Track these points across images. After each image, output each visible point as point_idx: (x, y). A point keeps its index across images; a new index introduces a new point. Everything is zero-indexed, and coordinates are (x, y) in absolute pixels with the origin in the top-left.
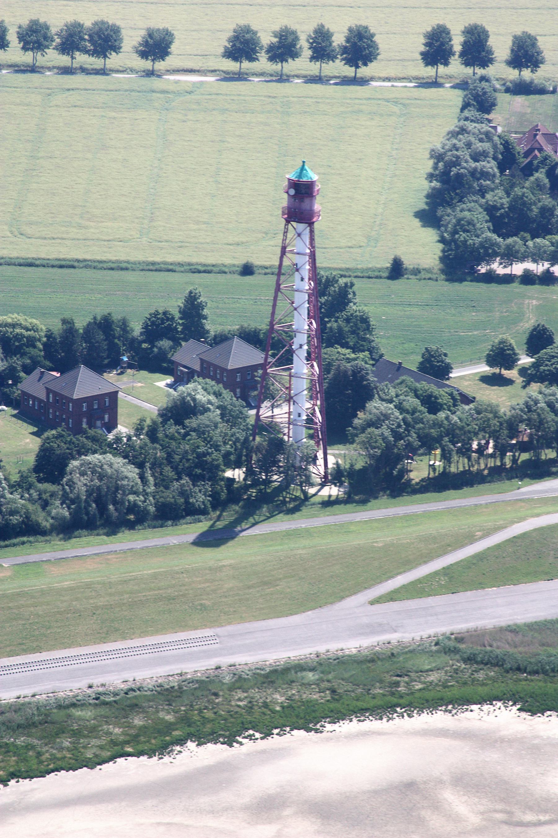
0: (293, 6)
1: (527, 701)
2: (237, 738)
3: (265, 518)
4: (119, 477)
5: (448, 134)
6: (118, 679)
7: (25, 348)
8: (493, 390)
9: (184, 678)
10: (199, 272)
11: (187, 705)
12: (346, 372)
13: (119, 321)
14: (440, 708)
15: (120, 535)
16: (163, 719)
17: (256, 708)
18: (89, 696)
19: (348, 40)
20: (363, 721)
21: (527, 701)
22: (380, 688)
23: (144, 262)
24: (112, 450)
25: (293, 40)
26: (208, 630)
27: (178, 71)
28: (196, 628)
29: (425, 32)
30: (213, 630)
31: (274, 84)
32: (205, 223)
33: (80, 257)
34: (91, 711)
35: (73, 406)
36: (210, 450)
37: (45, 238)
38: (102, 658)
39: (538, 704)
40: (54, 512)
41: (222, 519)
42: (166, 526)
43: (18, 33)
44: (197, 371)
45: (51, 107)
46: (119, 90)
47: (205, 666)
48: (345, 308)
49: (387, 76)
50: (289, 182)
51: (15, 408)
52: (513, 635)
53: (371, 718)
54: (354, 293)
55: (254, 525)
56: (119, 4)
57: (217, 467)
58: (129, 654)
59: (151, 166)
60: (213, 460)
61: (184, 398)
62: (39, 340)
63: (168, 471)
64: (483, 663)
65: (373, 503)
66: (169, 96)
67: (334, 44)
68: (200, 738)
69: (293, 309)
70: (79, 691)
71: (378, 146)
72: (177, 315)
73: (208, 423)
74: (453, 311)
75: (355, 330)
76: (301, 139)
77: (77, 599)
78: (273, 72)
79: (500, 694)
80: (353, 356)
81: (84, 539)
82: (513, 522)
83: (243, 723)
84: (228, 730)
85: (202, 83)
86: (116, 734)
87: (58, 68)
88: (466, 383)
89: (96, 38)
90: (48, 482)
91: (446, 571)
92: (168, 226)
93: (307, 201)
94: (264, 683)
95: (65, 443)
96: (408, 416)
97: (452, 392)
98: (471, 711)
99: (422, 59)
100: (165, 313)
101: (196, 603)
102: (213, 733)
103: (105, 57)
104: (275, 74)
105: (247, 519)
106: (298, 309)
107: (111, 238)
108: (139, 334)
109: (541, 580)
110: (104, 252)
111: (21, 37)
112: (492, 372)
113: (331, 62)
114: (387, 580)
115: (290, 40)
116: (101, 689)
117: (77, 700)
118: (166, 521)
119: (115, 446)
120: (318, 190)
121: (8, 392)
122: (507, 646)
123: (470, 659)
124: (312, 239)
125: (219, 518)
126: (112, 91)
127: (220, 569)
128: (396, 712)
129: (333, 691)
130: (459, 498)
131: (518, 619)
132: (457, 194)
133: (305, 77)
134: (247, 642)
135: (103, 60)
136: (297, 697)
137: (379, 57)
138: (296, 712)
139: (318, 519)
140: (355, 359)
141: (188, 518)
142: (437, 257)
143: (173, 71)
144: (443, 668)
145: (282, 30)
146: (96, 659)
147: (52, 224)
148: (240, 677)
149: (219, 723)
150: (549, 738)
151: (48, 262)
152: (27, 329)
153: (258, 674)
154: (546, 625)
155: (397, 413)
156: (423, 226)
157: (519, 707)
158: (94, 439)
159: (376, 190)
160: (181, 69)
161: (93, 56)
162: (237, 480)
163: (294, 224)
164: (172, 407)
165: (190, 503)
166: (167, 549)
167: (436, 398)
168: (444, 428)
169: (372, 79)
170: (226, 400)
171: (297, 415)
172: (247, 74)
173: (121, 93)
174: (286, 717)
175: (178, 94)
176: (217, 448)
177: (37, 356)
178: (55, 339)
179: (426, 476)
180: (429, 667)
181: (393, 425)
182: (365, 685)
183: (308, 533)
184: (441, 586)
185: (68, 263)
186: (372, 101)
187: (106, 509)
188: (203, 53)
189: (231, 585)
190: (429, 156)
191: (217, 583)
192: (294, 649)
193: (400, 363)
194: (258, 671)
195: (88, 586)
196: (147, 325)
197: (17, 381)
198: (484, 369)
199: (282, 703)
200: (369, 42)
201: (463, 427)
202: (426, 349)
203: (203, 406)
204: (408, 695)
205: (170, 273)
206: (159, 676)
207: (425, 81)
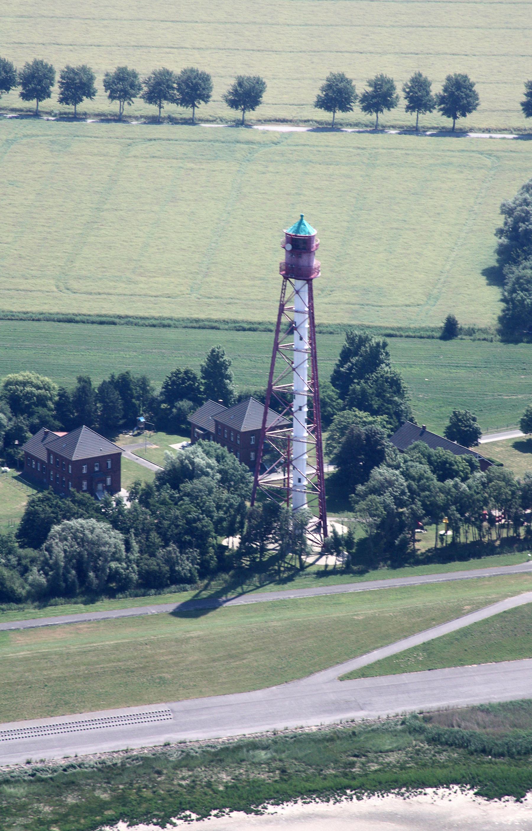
0: (405, 54)
1: (486, 785)
2: (172, 819)
3: (254, 588)
4: (98, 543)
5: (523, 188)
6: (59, 755)
7: (33, 407)
8: (524, 457)
9: (129, 754)
10: (244, 330)
11: (127, 783)
12: (359, 436)
13: (138, 381)
14: (393, 791)
15: (98, 604)
16: (99, 797)
17: (198, 787)
18: (26, 773)
19: (445, 90)
20: (309, 803)
21: (486, 785)
22: (333, 769)
23: (188, 319)
24: (99, 515)
25: (388, 89)
26: (163, 704)
27: (270, 121)
28: (150, 703)
29: (526, 81)
30: (169, 704)
31: (367, 135)
32: (261, 279)
33: (122, 313)
34: (24, 788)
35: (72, 468)
36: (201, 516)
37: (91, 294)
38: (46, 732)
39: (497, 788)
40: (30, 578)
41: (209, 588)
42: (149, 595)
43: (105, 81)
44: (212, 433)
45: (129, 157)
46: (203, 141)
47: (154, 742)
48: (375, 369)
49: (487, 127)
50: (287, 237)
51: (18, 470)
52: (484, 715)
53: (317, 800)
54: (387, 354)
55: (240, 595)
56: (224, 51)
57: (208, 534)
58: (76, 729)
59: (219, 219)
60: (203, 526)
61: (182, 462)
62: (51, 399)
63: (154, 536)
64: (447, 744)
65: (372, 573)
66: (254, 146)
67: (433, 94)
68: (133, 818)
69: (291, 369)
70: (16, 767)
71: (461, 200)
72: (199, 374)
73: (201, 487)
74: (501, 373)
75: (380, 393)
76: (382, 192)
77: (30, 670)
78: (368, 123)
79: (459, 777)
80: (371, 419)
81: (60, 607)
82: (506, 596)
83: (181, 803)
84: (164, 810)
85: (291, 133)
86: (45, 813)
87: (146, 117)
88: (498, 450)
89: (184, 86)
90: (30, 547)
91: (426, 647)
92: (221, 281)
93: (305, 257)
94: (212, 761)
95: (51, 507)
96: (413, 483)
97: (471, 459)
98: (425, 794)
99: (523, 109)
100: (186, 372)
101: (155, 676)
102: (148, 813)
103: (194, 106)
104: (371, 125)
105: (234, 589)
106: (296, 370)
107: (159, 293)
108: (159, 393)
109: (526, 657)
110: (149, 308)
111: (108, 85)
112: (527, 438)
113: (428, 112)
114: (361, 655)
115: (385, 89)
116: (39, 765)
117: (12, 777)
118: (148, 590)
119: (103, 510)
120: (317, 245)
121: (13, 453)
122: (476, 726)
123: (434, 740)
124: (311, 298)
125: (206, 588)
126: (195, 141)
127: (186, 641)
128: (345, 794)
129: (283, 771)
130: (461, 570)
131: (494, 698)
132: (524, 251)
133: (401, 127)
134: (203, 717)
135: (191, 110)
136: (244, 777)
137: (478, 108)
138: (239, 793)
139: (309, 590)
140: (370, 423)
141: (173, 586)
142: (495, 317)
143: (265, 121)
144: (404, 749)
145: (377, 79)
146: (40, 733)
147: (100, 279)
148: (188, 754)
149: (156, 803)
150: (501, 824)
151: (88, 318)
152: (38, 388)
153: (207, 752)
154: (522, 705)
155: (402, 480)
156: (489, 284)
157: (476, 790)
158: (81, 503)
159: (449, 246)
160: (273, 118)
161: (181, 105)
162: (230, 547)
163: (292, 280)
164: (170, 470)
165: (175, 571)
166: (143, 619)
167: (451, 464)
168: (451, 496)
169: (471, 130)
170: (228, 464)
171: (297, 480)
172: (341, 125)
173: (204, 143)
174: (228, 797)
175: (262, 144)
176: (209, 514)
177: (45, 416)
178: (67, 397)
179: (434, 546)
180: (390, 747)
181: (396, 492)
182: (318, 765)
183: (295, 604)
184: (418, 662)
185: (109, 319)
186: (465, 154)
187: (86, 576)
188: (299, 103)
189: (196, 658)
190: (499, 211)
191: (181, 655)
192: (251, 726)
193: (424, 428)
194: (209, 749)
195: (44, 656)
196: (168, 385)
197: (23, 440)
198: (519, 435)
199: (227, 782)
200: (468, 92)
201: (472, 495)
202: (454, 412)
203: (201, 470)
204: (360, 776)
205: (214, 331)
206: (102, 752)
207: (526, 133)
